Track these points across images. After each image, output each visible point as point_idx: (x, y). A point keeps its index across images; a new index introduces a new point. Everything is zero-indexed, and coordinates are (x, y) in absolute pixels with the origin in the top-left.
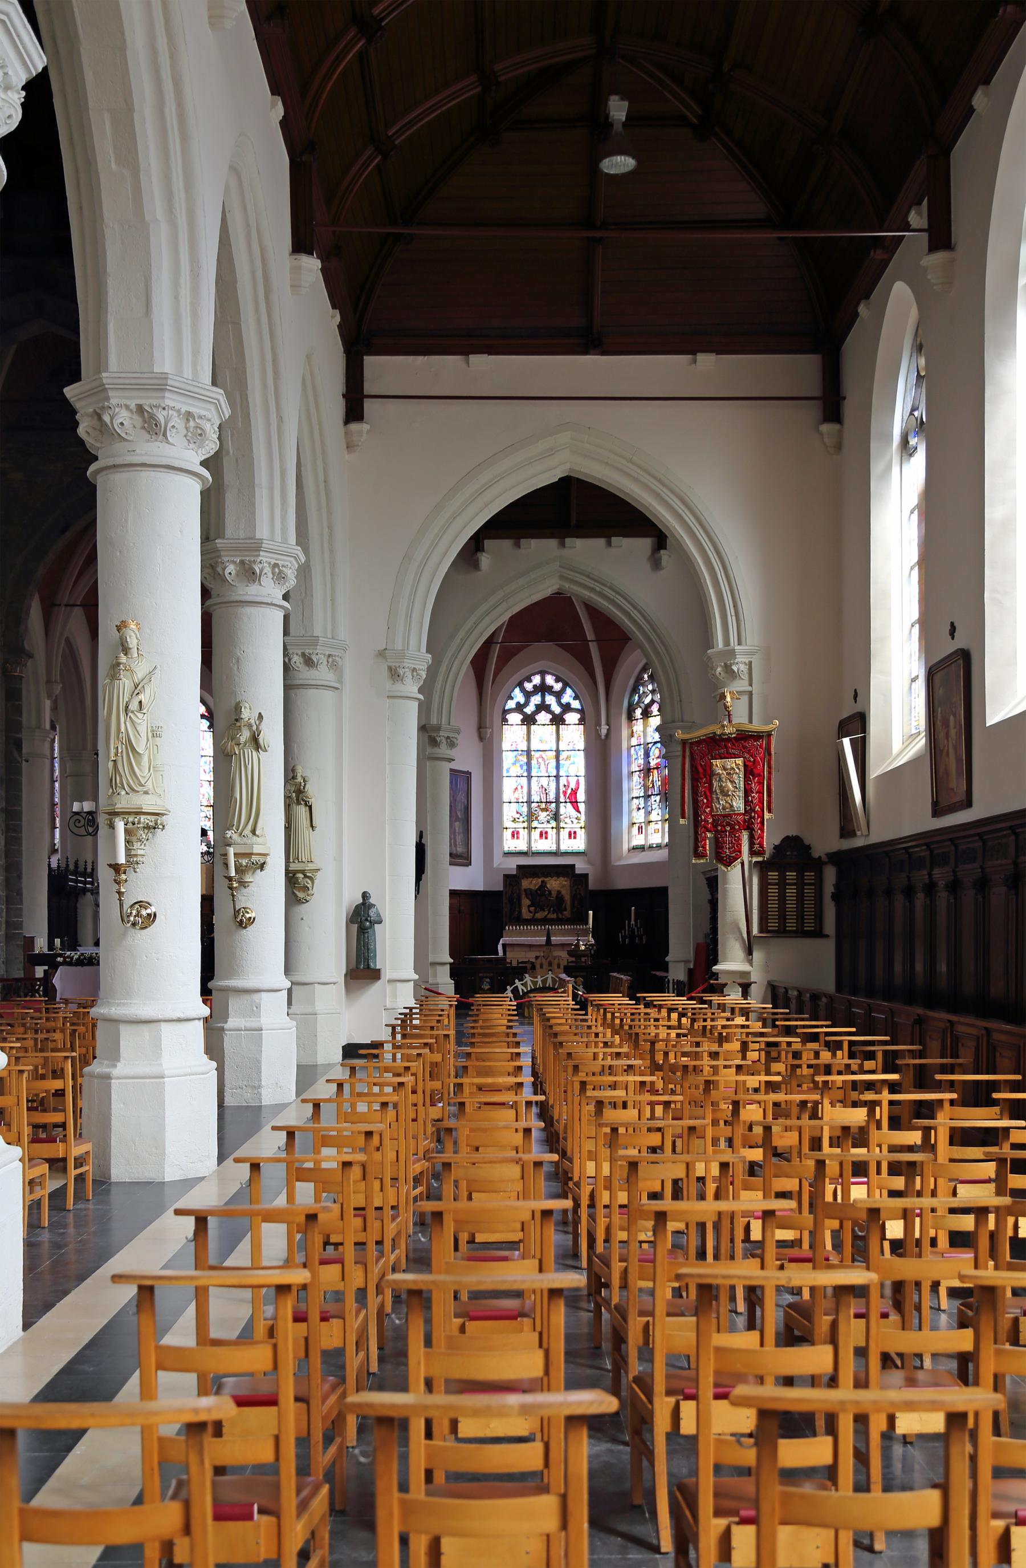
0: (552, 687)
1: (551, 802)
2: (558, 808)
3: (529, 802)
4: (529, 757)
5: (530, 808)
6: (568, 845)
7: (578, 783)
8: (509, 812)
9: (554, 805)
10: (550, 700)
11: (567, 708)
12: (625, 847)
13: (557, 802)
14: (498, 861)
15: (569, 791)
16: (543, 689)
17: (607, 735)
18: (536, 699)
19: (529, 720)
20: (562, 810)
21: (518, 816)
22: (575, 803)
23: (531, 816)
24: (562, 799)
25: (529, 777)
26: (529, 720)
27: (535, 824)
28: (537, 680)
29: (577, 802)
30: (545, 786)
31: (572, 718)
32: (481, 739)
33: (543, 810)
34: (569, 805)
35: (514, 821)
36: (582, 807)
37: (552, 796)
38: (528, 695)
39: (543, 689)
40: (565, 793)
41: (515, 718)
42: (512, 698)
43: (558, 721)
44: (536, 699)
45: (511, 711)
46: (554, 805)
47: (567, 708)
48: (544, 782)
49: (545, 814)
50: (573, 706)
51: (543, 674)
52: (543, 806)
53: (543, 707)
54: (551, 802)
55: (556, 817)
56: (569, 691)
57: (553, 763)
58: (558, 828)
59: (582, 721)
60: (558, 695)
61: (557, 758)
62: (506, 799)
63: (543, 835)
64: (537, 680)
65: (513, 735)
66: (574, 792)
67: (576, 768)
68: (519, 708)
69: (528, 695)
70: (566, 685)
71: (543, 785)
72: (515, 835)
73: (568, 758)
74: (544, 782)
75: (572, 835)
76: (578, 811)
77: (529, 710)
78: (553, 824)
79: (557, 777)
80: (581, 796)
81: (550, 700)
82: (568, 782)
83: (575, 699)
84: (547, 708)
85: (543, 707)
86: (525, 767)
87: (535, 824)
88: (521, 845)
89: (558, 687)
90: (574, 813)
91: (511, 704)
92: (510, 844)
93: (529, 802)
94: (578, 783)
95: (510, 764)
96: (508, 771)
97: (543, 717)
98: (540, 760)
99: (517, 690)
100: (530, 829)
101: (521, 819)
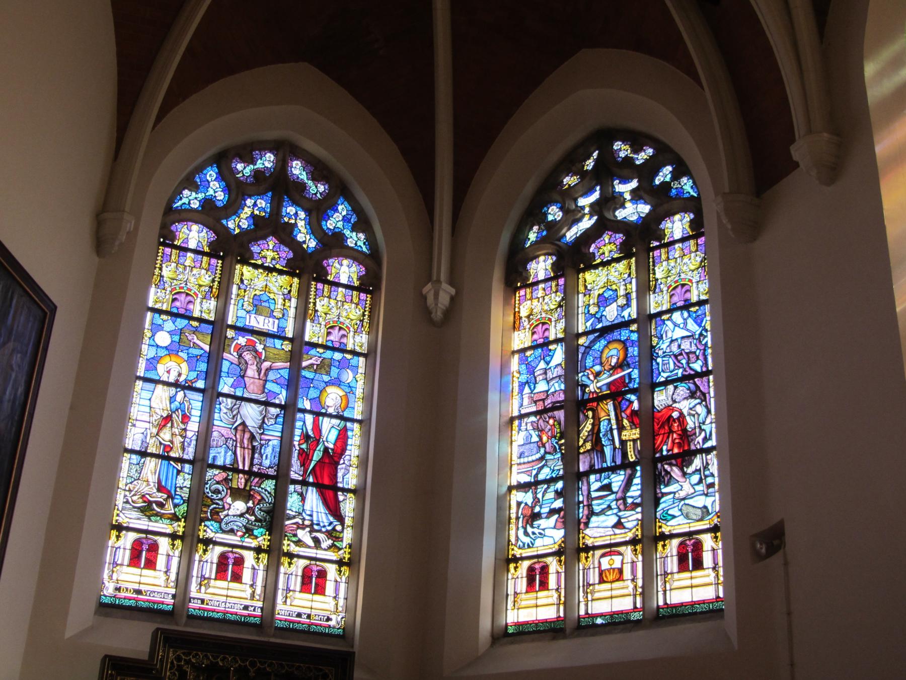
0: (302, 186)
1: (264, 476)
2: (280, 496)
3: (201, 463)
4: (219, 342)
5: (199, 481)
6: (296, 605)
7: (343, 436)
8: (136, 479)
9: (269, 485)
10: (294, 215)
11: (333, 244)
12: (485, 624)
13: (281, 477)
14: (79, 616)
15: (317, 456)
16: (279, 186)
17: (449, 313)
18: (256, 205)
19: (230, 251)
20: (293, 502)
21: (160, 497)
22: (330, 493)
23: (201, 506)
24: (295, 472)
25: (211, 395)
26: (230, 251)
27: (209, 530)
28: (267, 161)
29: (335, 489)
30: (252, 424)
31: (345, 271)
32: (101, 242)
33: (237, 494)
34: (312, 495)
35: (147, 509)
36: (348, 506)
37: (268, 459)
38: (238, 191)
39: (279, 186)
40: (305, 457)
41: (194, 235)
42: (195, 188)
43: (307, 269)
44: (256, 205)
45: (187, 216)
46: (269, 485)
47: (333, 244)
48: (251, 414)
49: (240, 506)
50: (350, 243)
51: (286, 150)
52: (240, 481)
53: (271, 226)
54: (264, 476)
55: (274, 519)
56: (343, 209)
57: (282, 368)
58: (274, 554)
59: (367, 285)
60: (317, 211)
61: (295, 358)
62: (133, 438)
63: (228, 567)
64: (267, 161)
65: (183, 275)
66: (332, 459)
67: (345, 398)
68: (210, 214)
69: (238, 191)
70: (340, 189)
71: (245, 417)
72: (143, 554)
73: (324, 366)
74: (251, 414)
75: (313, 581)
76: (340, 519)
77: (239, 223)
78: (262, 538)
79: (289, 410)
80: (348, 476)
81: (294, 215)
82: (317, 428)
83: (354, 229)
84: (285, 234)
85: (271, 226)
86: (203, 366)
87: (209, 530)
88: (156, 584)
89: (317, 189)
90: (322, 516)
91: (191, 199)
92: (122, 579)
93: (201, 463)
94: (343, 436)
95: (162, 355)
96: (152, 364)
97: (269, 251)
98: (248, 356)
99: (211, 174)
100: (191, 541)
101: (169, 509)
